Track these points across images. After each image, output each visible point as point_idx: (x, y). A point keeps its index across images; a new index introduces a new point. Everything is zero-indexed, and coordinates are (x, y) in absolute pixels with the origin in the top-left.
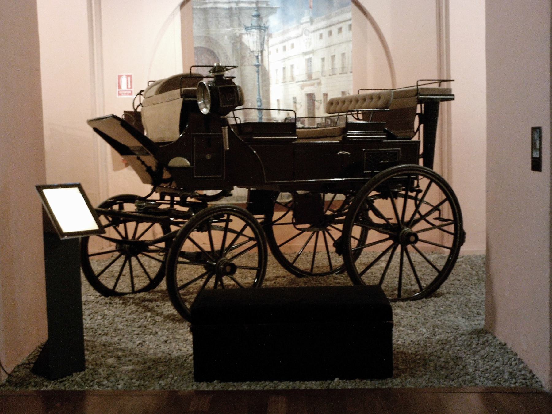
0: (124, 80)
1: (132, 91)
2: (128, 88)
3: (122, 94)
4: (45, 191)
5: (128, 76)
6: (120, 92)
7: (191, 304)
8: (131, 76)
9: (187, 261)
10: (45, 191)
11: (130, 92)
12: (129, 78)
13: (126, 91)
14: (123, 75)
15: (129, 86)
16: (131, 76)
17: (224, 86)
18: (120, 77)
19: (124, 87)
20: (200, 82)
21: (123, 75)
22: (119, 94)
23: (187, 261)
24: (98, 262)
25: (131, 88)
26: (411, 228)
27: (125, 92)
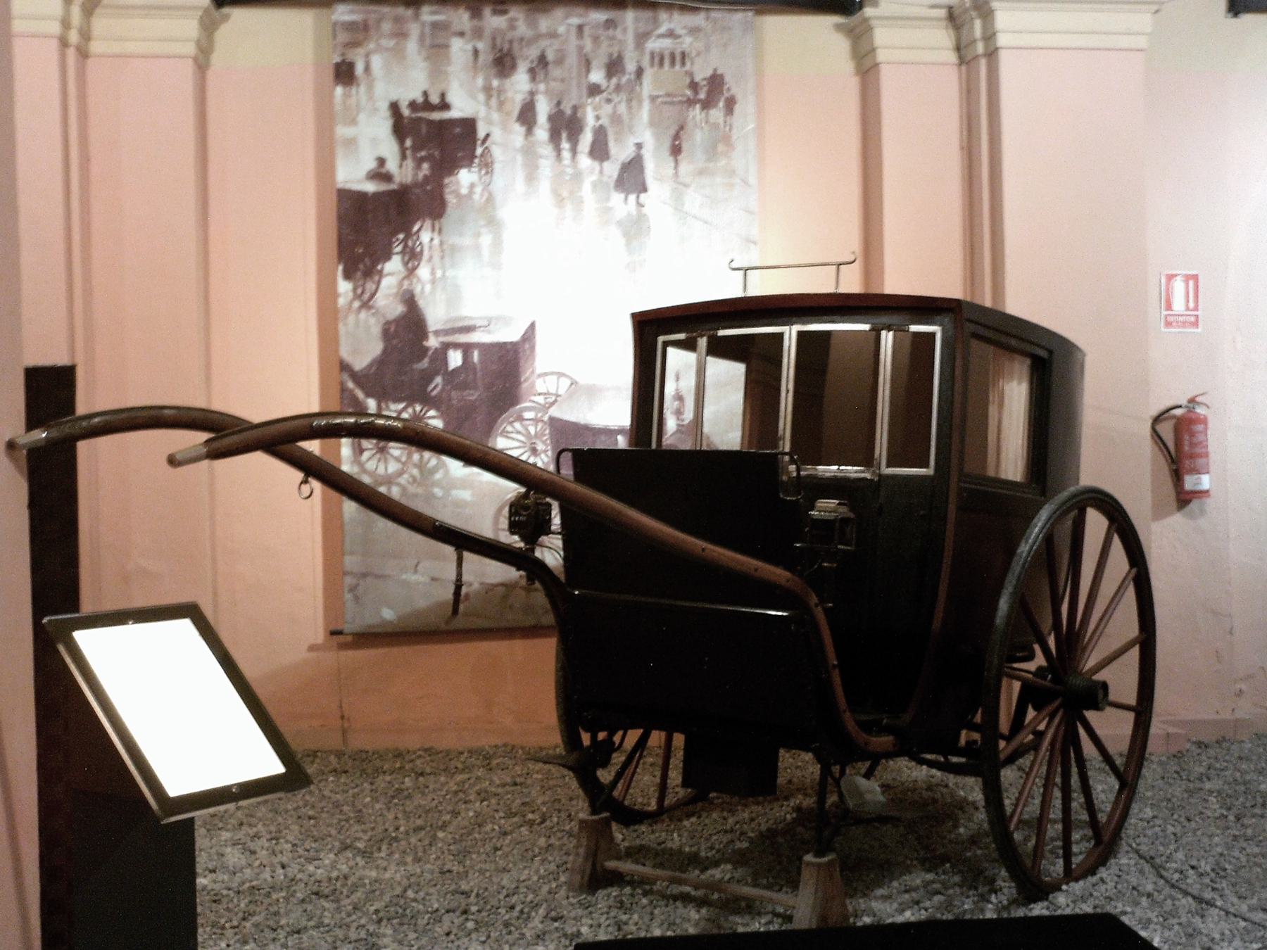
0: (1179, 286)
1: (1197, 316)
2: (1187, 308)
3: (1174, 324)
4: (273, 766)
5: (1187, 278)
6: (1171, 319)
7: (382, 444)
8: (1195, 278)
9: (1082, 732)
10: (273, 766)
11: (1193, 319)
12: (1191, 283)
13: (1182, 315)
14: (1176, 275)
15: (1191, 305)
16: (1195, 278)
17: (53, 618)
18: (1170, 277)
19: (1179, 305)
20: (548, 500)
21: (1176, 275)
22: (1168, 324)
23: (1082, 732)
24: (521, 936)
25: (1196, 308)
26: (1078, 484)
27: (1181, 319)
